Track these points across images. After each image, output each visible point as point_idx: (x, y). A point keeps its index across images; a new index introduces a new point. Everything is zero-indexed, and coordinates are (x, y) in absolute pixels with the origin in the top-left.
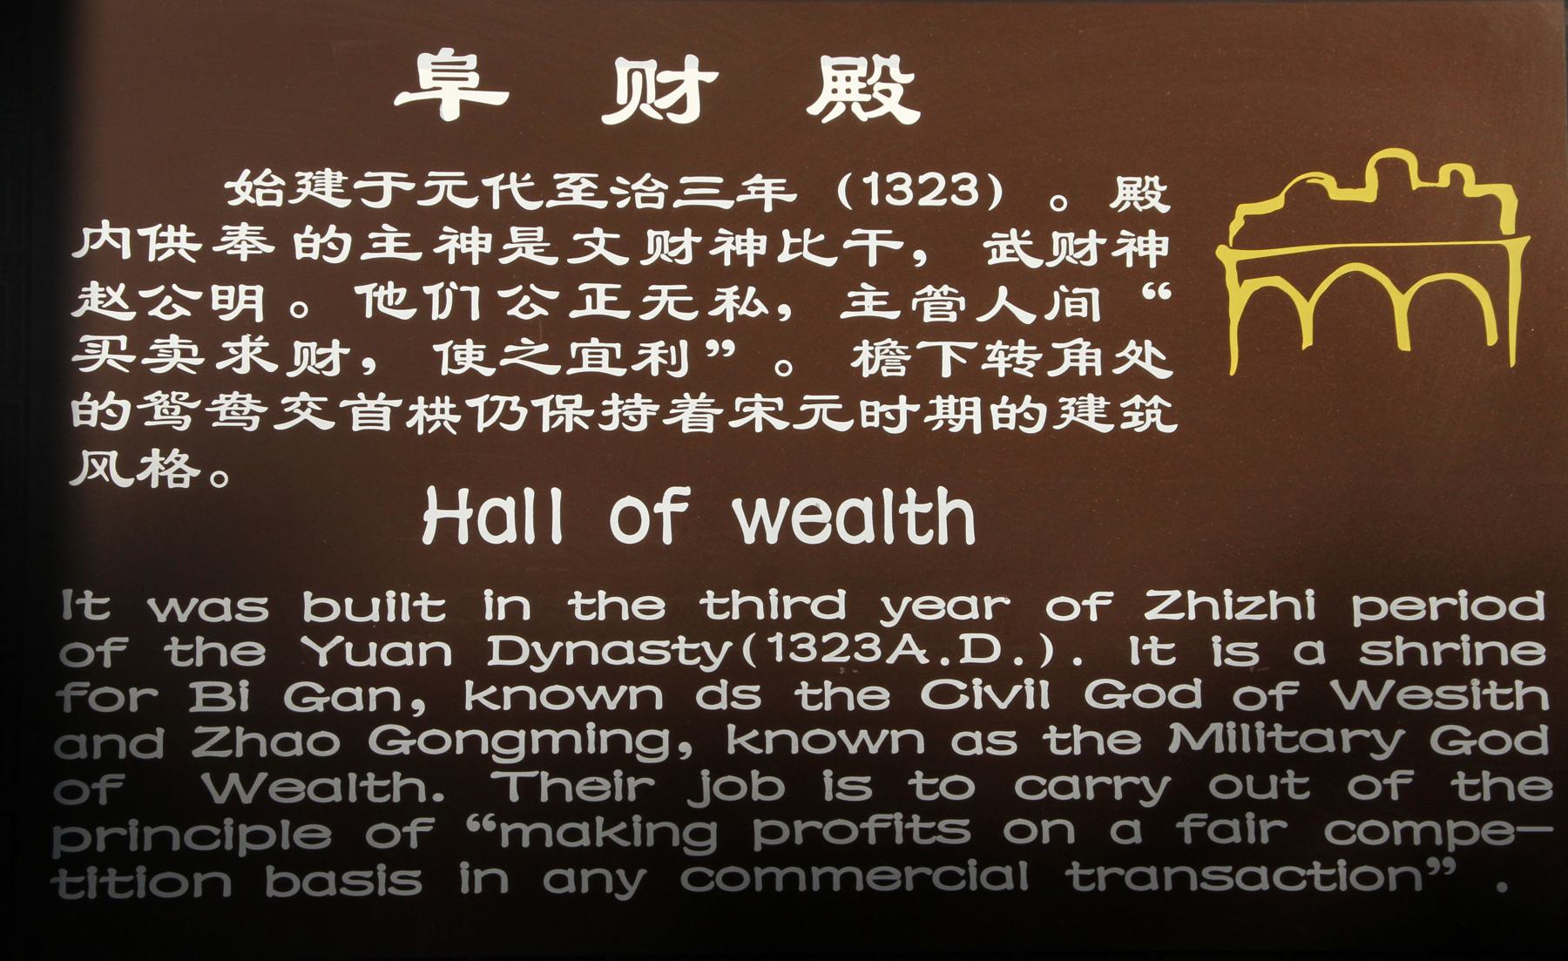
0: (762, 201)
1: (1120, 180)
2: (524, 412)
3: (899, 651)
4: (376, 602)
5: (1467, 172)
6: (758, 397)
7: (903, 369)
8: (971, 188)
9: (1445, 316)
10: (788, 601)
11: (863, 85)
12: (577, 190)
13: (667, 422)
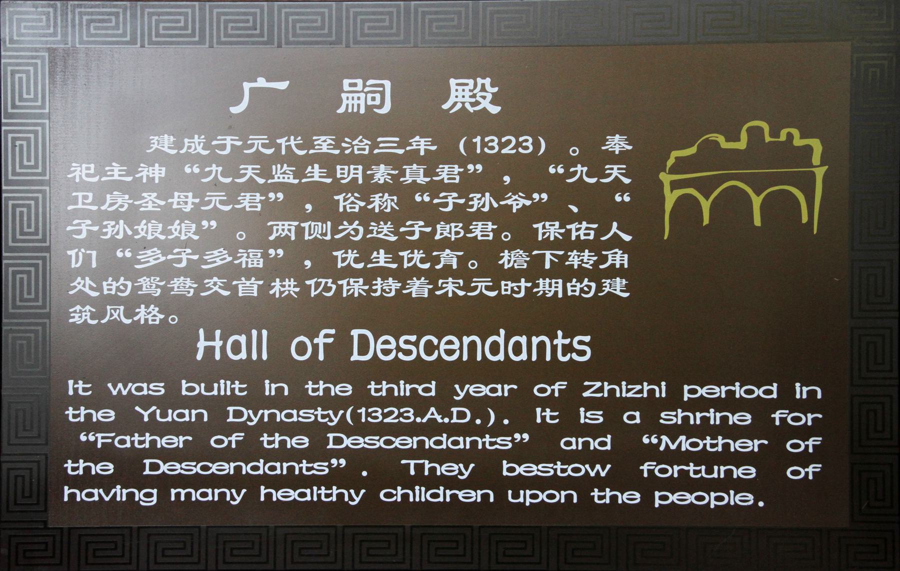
0: (419, 150)
1: (453, 82)
2: (334, 287)
3: (428, 416)
4: (216, 385)
5: (795, 132)
6: (450, 279)
7: (526, 264)
8: (529, 144)
9: (781, 209)
10: (408, 387)
11: (471, 94)
12: (325, 145)
13: (405, 292)
